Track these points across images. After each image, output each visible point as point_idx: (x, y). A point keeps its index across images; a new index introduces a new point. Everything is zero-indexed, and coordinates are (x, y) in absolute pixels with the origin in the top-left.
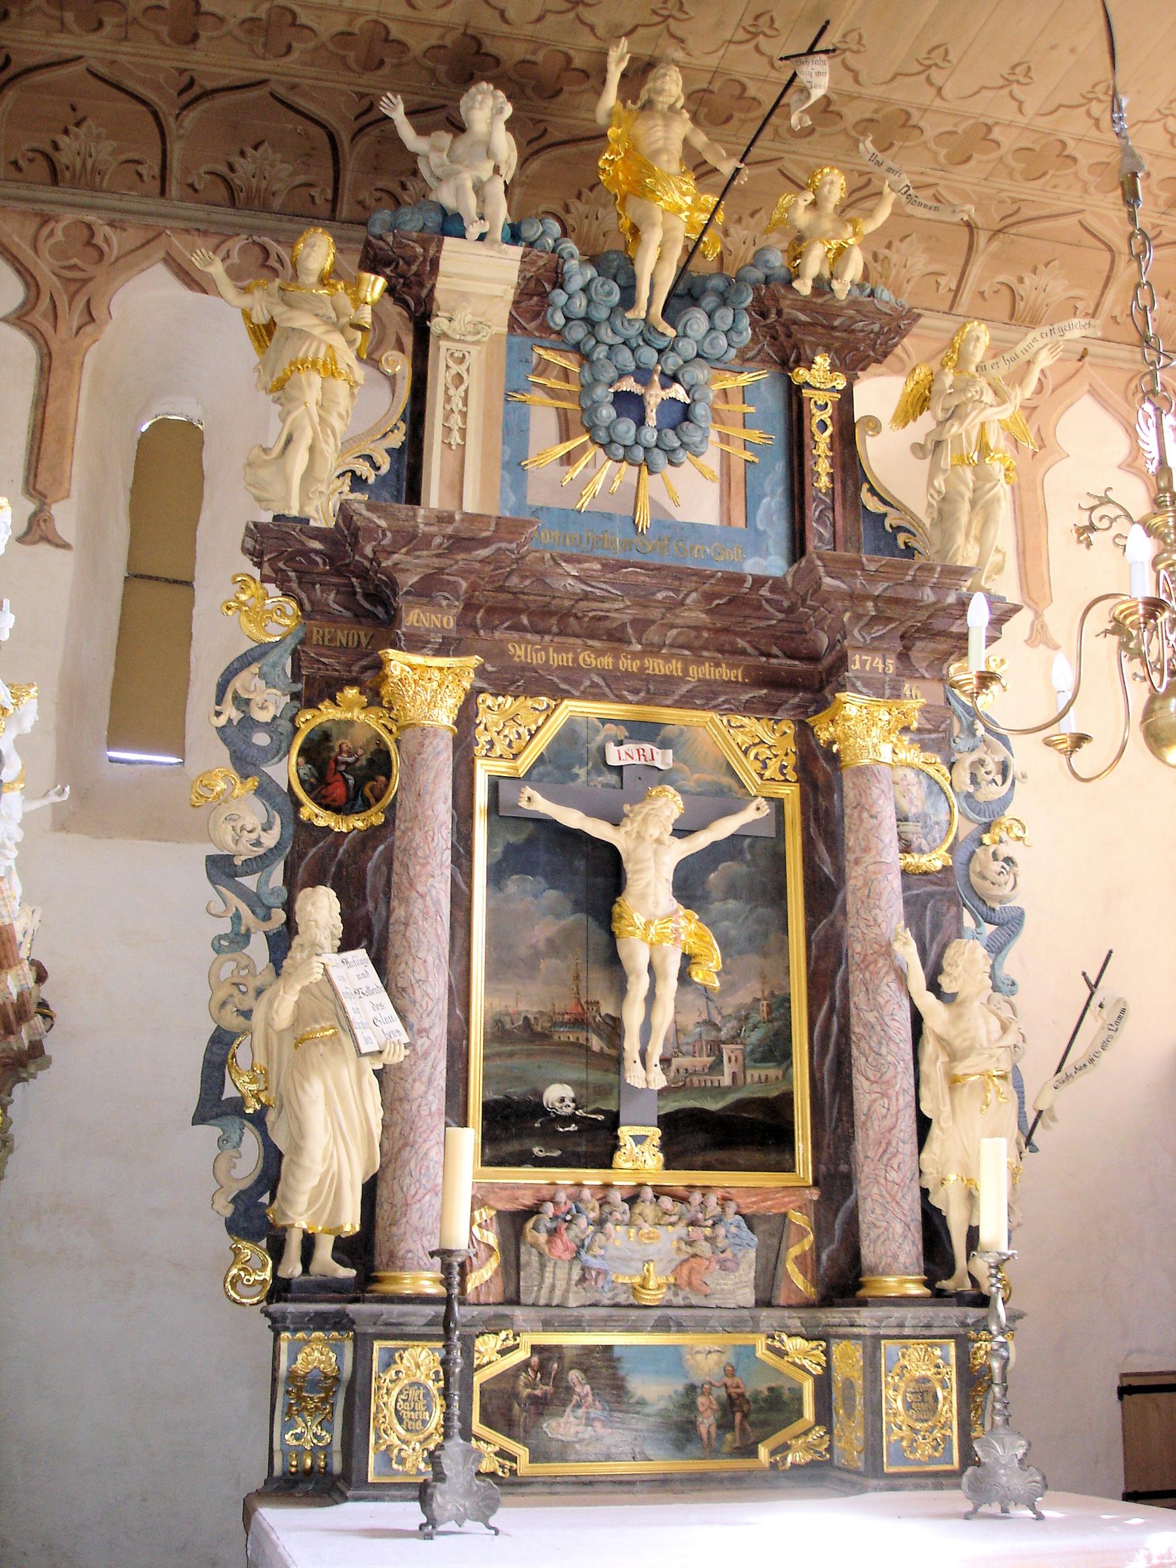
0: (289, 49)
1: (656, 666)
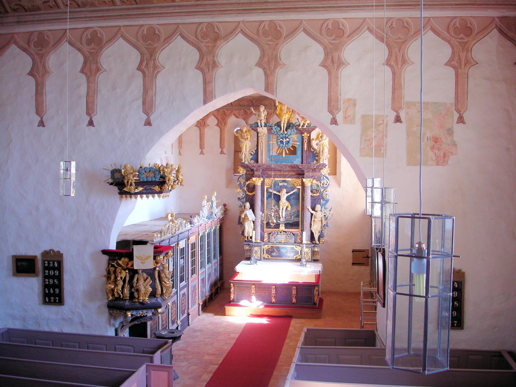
1: (285, 173)
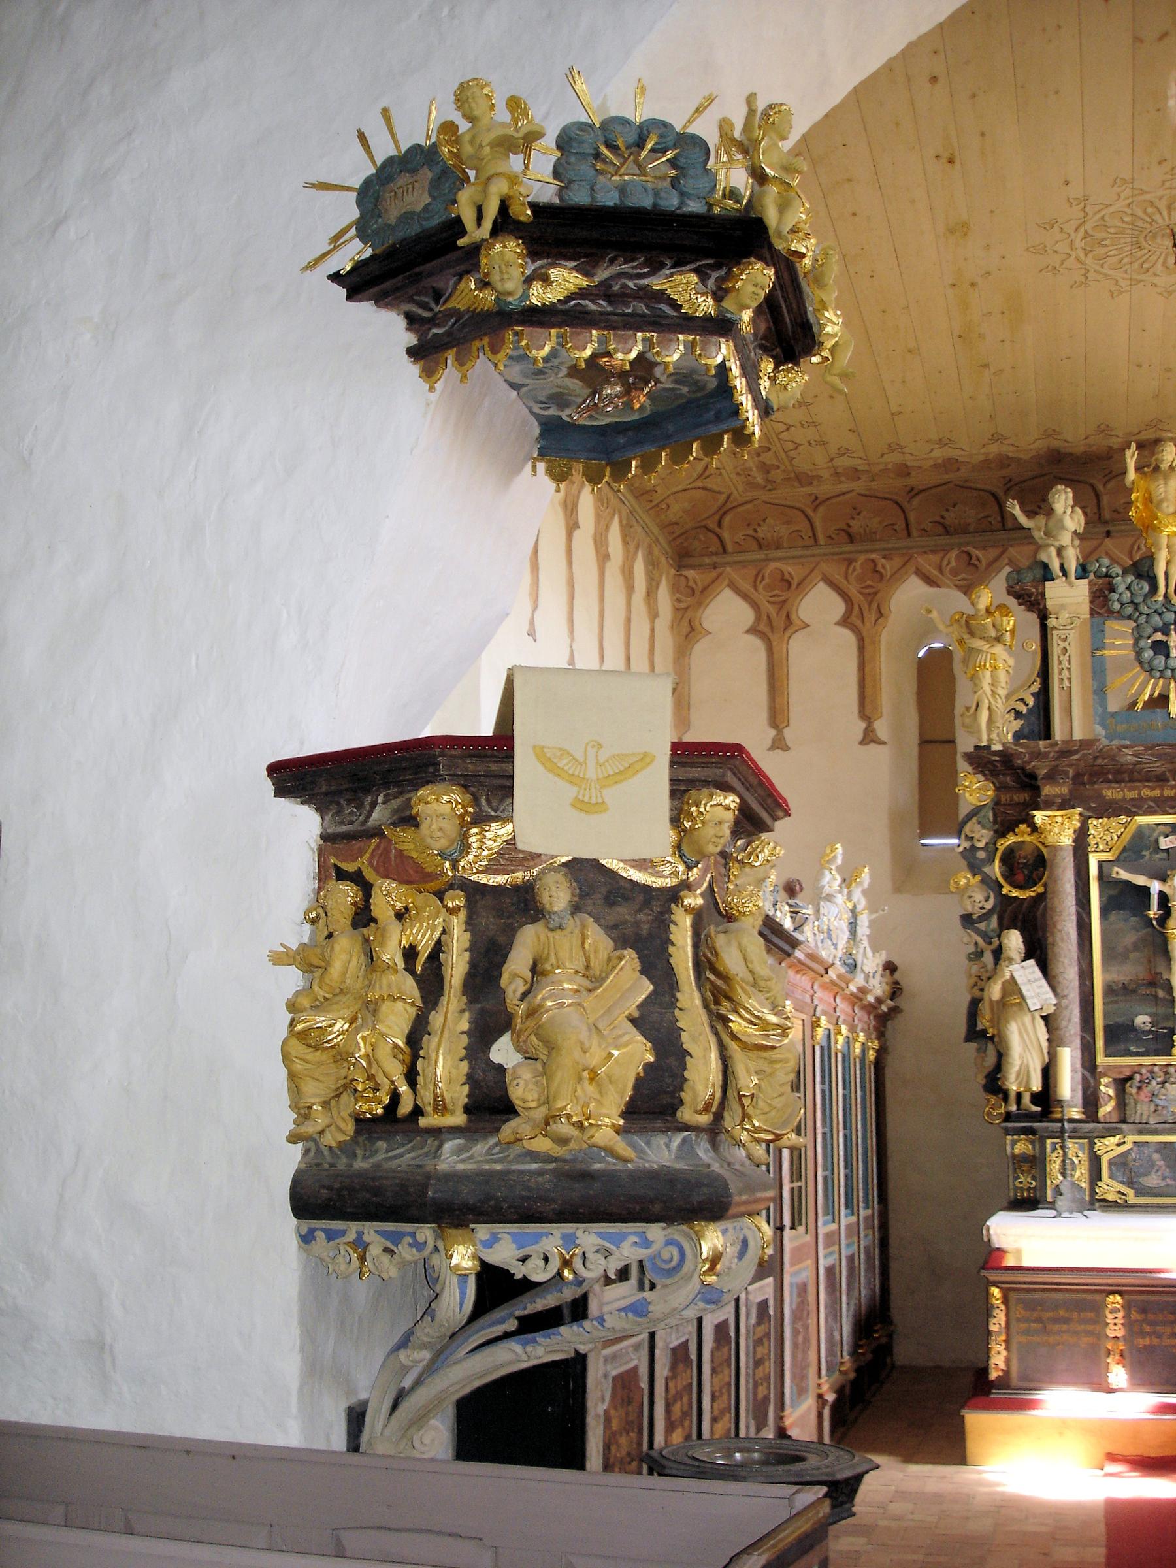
0: (958, 469)
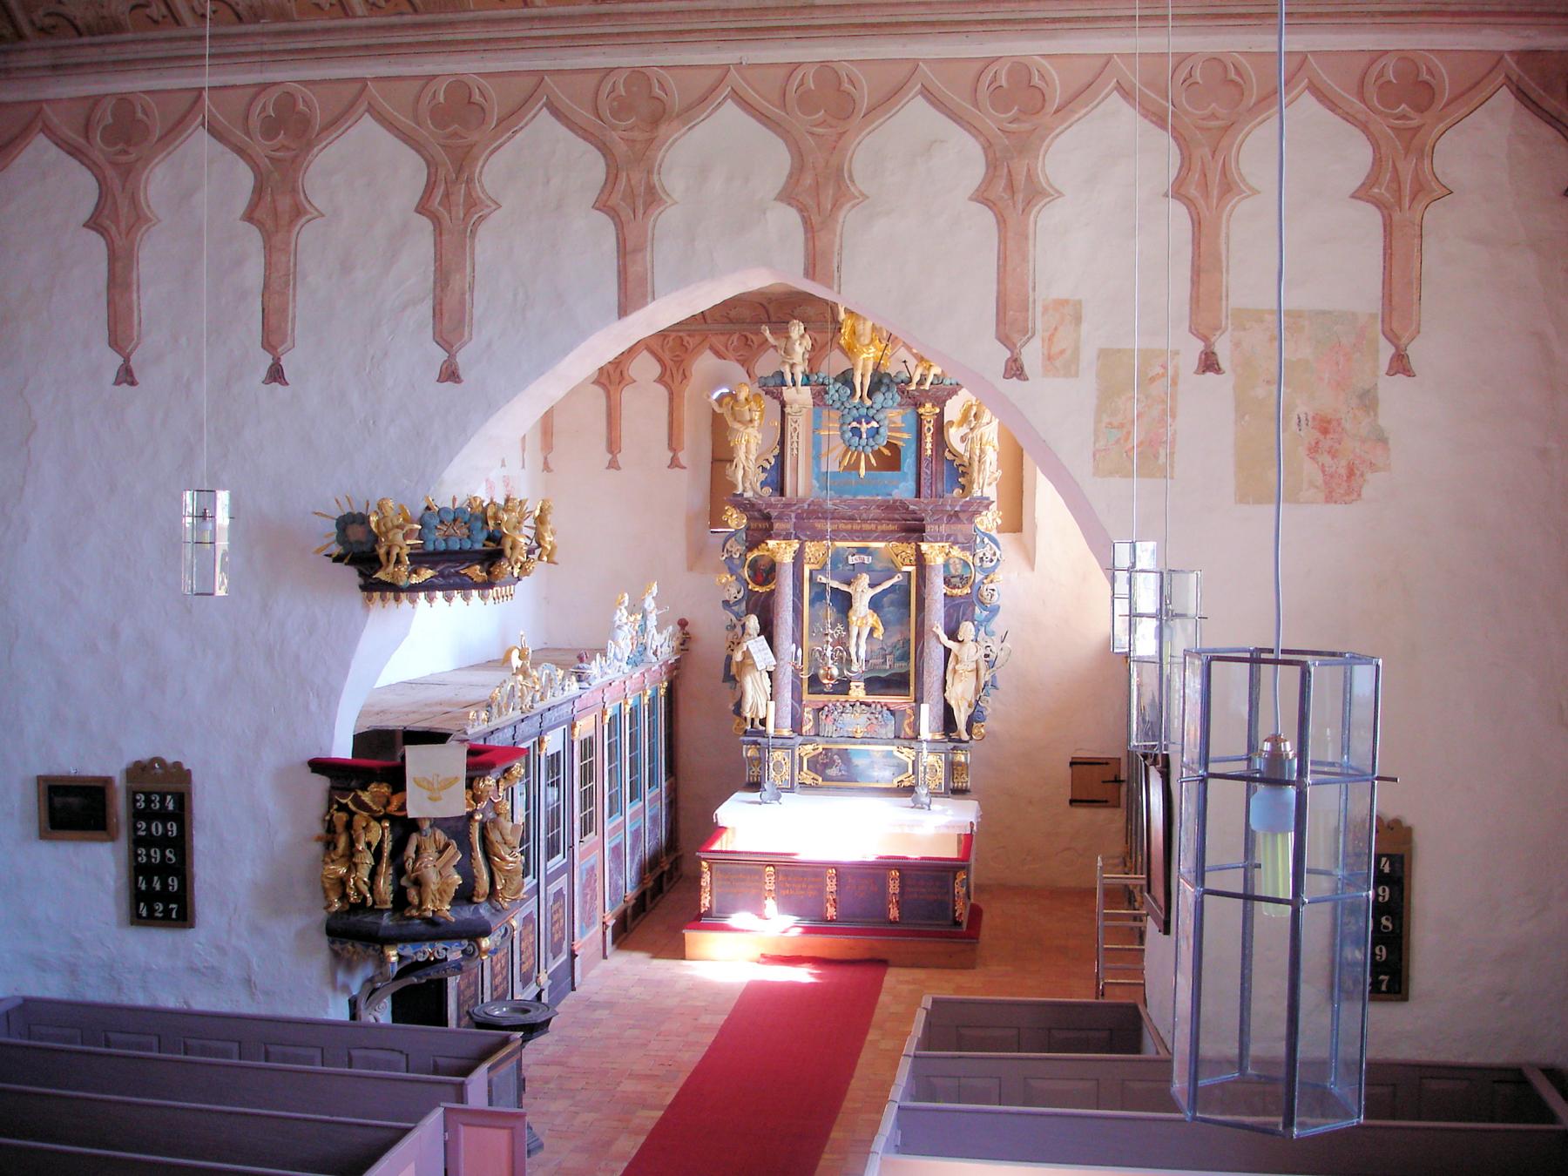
1: (866, 527)
